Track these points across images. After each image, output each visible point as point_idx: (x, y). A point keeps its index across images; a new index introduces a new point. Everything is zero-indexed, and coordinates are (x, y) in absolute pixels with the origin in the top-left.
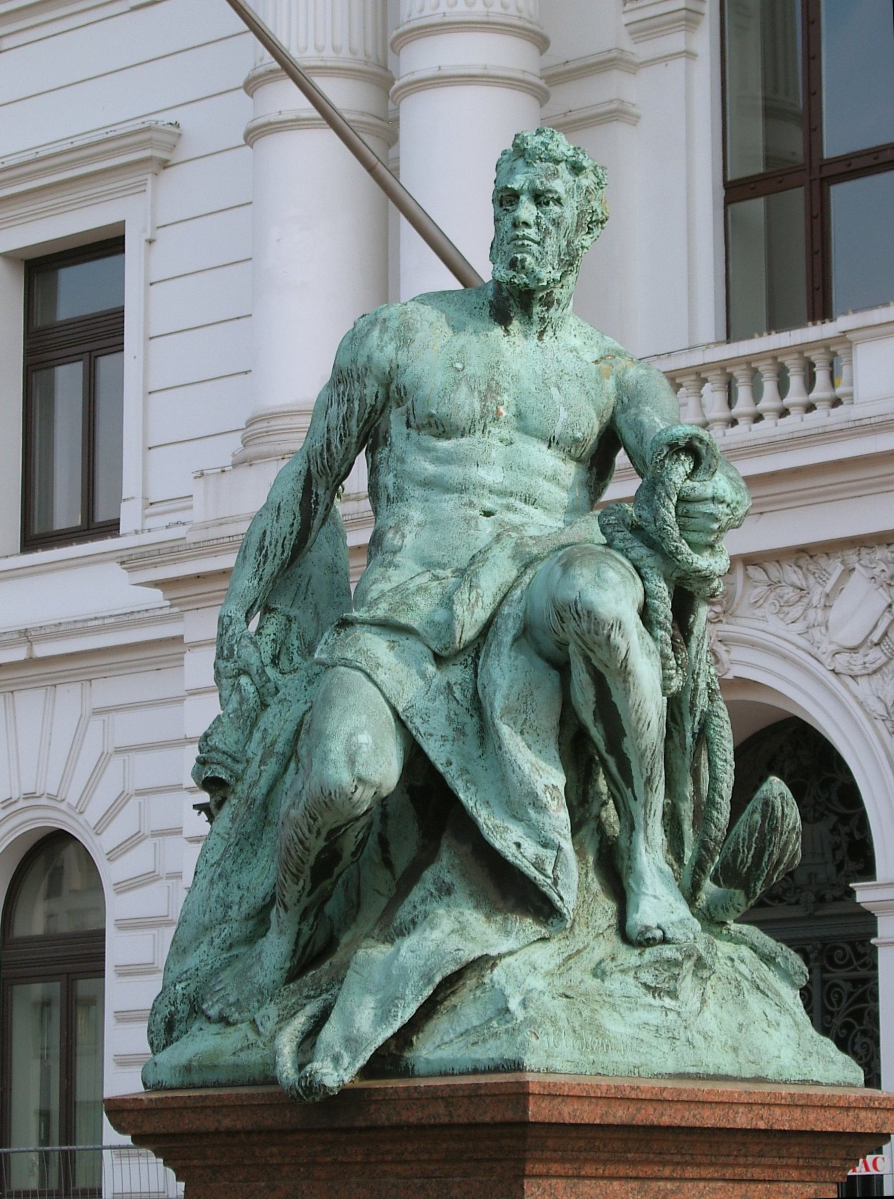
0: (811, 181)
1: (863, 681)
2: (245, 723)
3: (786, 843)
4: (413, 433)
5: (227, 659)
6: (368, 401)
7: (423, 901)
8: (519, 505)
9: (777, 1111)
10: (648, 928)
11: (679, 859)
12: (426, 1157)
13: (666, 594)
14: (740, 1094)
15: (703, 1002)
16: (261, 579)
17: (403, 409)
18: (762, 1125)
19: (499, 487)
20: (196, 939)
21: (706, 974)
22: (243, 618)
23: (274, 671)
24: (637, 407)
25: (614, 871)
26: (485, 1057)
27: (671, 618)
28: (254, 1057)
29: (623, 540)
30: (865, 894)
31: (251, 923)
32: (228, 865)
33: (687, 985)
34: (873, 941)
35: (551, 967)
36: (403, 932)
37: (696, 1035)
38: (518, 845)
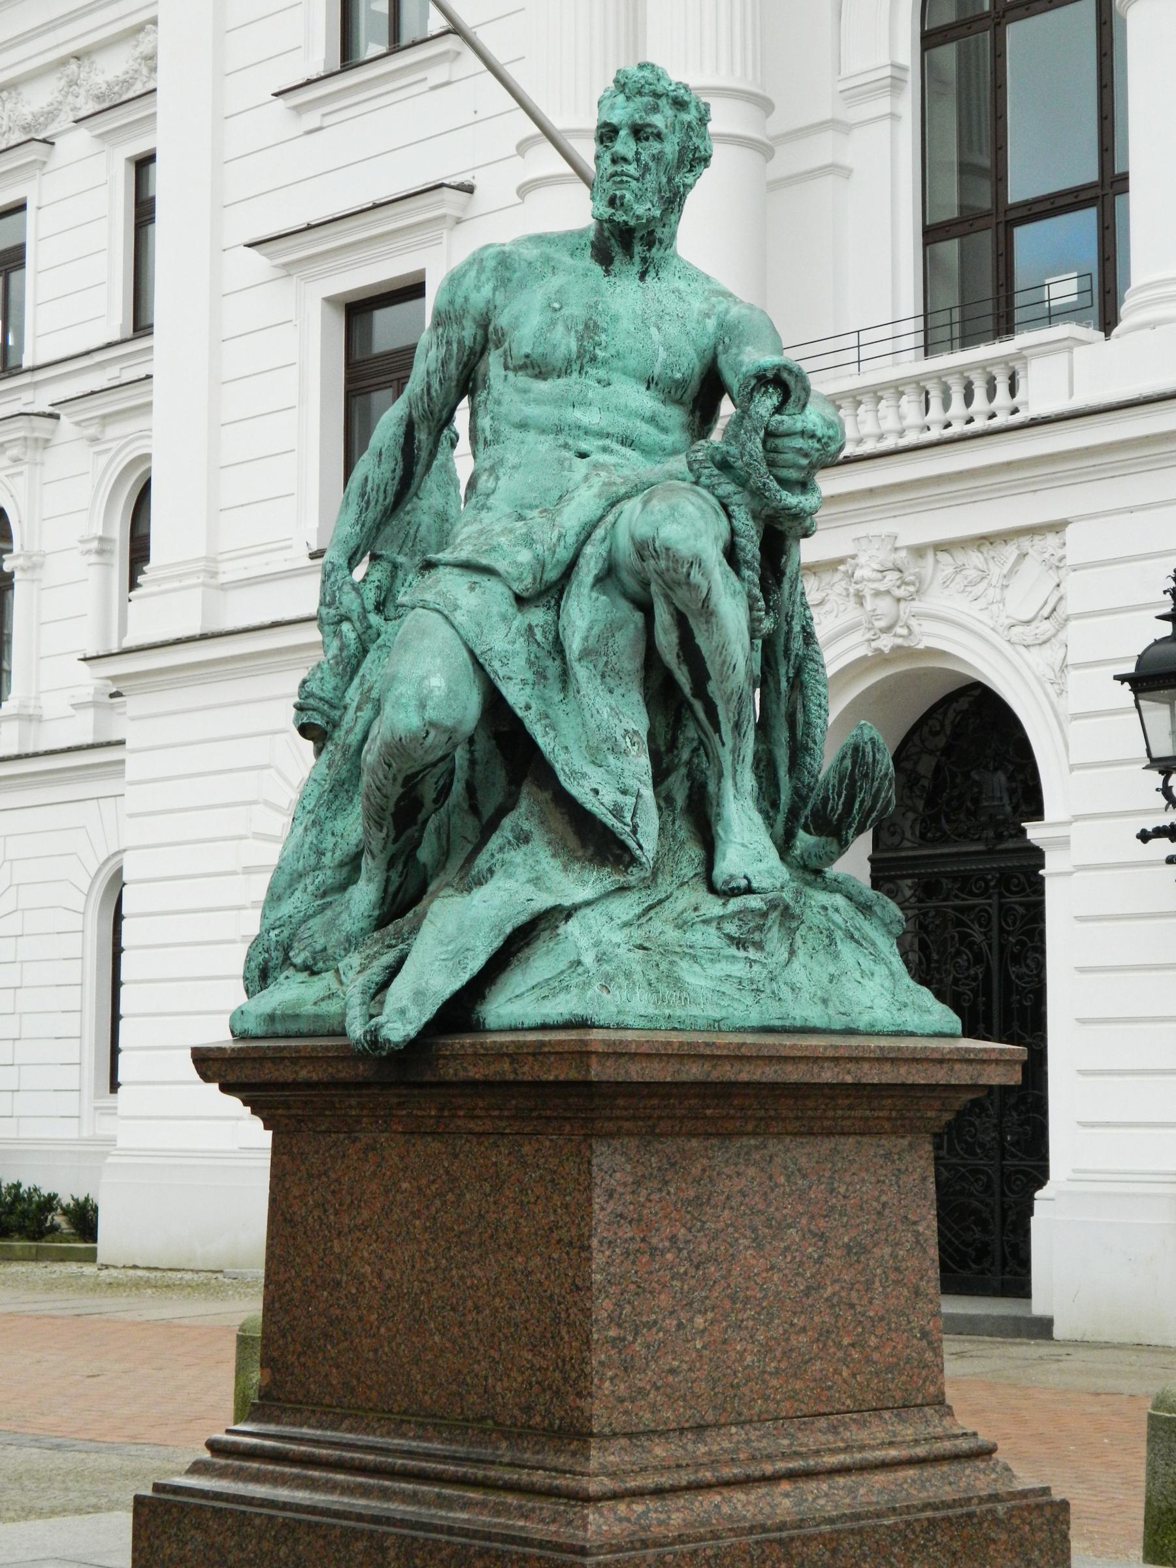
0: (997, 224)
1: (1034, 650)
2: (344, 670)
3: (879, 790)
4: (511, 374)
5: (329, 605)
6: (467, 343)
7: (501, 849)
8: (616, 446)
9: (866, 1066)
10: (732, 877)
11: (775, 805)
12: (496, 1113)
13: (753, 532)
14: (825, 1048)
15: (792, 952)
16: (363, 525)
17: (501, 349)
18: (849, 1079)
19: (596, 428)
20: (290, 886)
21: (794, 924)
22: (345, 565)
23: (377, 618)
24: (738, 347)
25: (700, 819)
26: (554, 1012)
27: (759, 557)
28: (333, 1007)
29: (710, 476)
30: (1034, 832)
31: (345, 870)
32: (322, 812)
33: (774, 937)
34: (1041, 872)
35: (629, 917)
36: (480, 882)
37: (782, 986)
38: (596, 792)
